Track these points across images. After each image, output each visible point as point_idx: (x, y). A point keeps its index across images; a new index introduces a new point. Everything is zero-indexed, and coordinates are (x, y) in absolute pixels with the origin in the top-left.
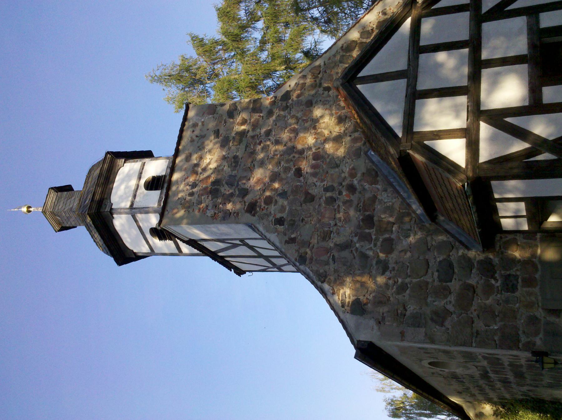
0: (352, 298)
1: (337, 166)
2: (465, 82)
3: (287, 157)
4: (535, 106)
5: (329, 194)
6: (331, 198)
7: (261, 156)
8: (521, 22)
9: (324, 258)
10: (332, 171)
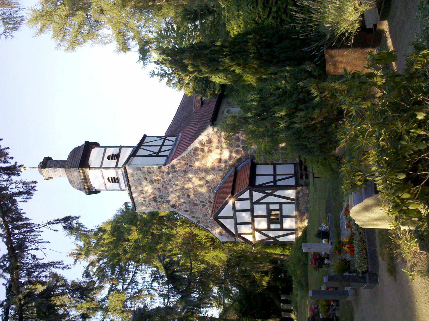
2: (250, 221)
4: (269, 229)
6: (204, 204)
7: (171, 190)
8: (264, 206)
9: (206, 221)
10: (202, 196)
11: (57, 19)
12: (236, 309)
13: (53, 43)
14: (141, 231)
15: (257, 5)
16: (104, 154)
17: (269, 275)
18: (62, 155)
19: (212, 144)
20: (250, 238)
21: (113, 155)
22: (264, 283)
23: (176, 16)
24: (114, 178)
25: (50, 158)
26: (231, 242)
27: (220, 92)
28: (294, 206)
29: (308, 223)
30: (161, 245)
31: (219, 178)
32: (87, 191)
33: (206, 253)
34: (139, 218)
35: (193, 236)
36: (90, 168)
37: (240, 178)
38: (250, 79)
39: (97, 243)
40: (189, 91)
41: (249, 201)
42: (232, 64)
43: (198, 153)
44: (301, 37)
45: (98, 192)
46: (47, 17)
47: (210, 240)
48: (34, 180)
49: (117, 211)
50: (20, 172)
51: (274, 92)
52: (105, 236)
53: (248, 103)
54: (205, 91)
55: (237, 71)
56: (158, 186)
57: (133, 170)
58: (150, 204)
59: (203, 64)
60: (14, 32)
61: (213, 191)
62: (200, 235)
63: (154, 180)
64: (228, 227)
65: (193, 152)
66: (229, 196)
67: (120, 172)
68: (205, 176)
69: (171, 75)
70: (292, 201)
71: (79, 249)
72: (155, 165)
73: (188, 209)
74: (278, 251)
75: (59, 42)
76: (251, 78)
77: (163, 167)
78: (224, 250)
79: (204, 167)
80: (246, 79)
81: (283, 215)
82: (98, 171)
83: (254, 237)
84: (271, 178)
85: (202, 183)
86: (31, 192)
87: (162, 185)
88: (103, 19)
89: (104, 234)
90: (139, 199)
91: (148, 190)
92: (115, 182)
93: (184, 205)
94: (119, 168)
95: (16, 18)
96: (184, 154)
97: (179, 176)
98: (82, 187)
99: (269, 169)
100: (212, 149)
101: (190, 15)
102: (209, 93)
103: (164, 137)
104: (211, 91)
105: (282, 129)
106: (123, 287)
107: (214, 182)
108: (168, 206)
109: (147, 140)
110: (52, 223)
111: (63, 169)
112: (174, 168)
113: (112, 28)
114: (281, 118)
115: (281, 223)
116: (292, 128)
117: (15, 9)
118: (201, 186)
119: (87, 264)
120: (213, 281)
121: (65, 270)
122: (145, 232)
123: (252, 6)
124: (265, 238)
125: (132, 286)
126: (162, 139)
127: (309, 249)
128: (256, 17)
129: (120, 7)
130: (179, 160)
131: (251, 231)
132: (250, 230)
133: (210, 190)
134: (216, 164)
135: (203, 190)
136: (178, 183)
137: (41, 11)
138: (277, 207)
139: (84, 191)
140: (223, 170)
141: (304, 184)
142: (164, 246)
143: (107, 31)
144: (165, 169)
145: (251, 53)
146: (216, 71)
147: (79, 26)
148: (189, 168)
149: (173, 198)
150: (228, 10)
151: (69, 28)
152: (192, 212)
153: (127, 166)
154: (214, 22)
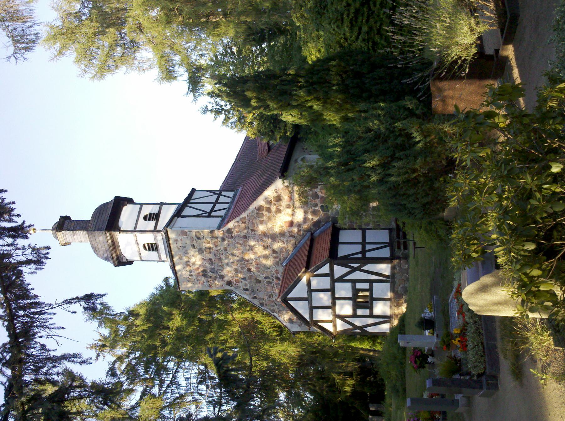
1: (269, 269)
4: (355, 316)
5: (267, 280)
7: (226, 261)
8: (349, 285)
9: (272, 304)
10: (267, 270)
13: (76, 69)
14: (185, 316)
16: (139, 214)
18: (85, 213)
19: (281, 202)
20: (329, 327)
21: (150, 214)
22: (347, 389)
24: (152, 244)
25: (68, 218)
27: (293, 135)
28: (388, 285)
29: (407, 308)
30: (212, 335)
31: (290, 247)
33: (270, 347)
34: (183, 298)
35: (254, 324)
36: (120, 231)
37: (317, 247)
38: (332, 118)
39: (127, 331)
40: (252, 133)
41: (328, 278)
42: (309, 98)
44: (399, 66)
45: (130, 263)
46: (69, 36)
47: (277, 329)
48: (46, 245)
50: (28, 235)
51: (364, 135)
52: (138, 322)
54: (273, 132)
55: (315, 107)
56: (209, 256)
57: (176, 235)
58: (198, 280)
59: (271, 98)
60: (27, 52)
61: (281, 264)
62: (264, 322)
63: (204, 248)
65: (256, 211)
66: (303, 270)
68: (272, 244)
69: (228, 111)
70: (386, 279)
71: (102, 339)
73: (248, 287)
74: (366, 345)
77: (216, 232)
79: (271, 232)
80: (328, 118)
81: (374, 296)
82: (130, 236)
83: (335, 326)
84: (359, 248)
85: (267, 252)
86: (43, 260)
90: (184, 272)
91: (195, 262)
92: (153, 250)
93: (244, 282)
94: (159, 231)
96: (244, 215)
97: (237, 243)
98: (110, 256)
99: (356, 236)
100: (281, 208)
101: (255, 35)
103: (218, 192)
104: (281, 132)
105: (373, 183)
106: (160, 390)
108: (222, 283)
109: (196, 195)
110: (69, 303)
112: (231, 233)
115: (371, 308)
116: (386, 182)
117: (29, 24)
118: (266, 257)
119: (113, 359)
121: (83, 365)
123: (336, 24)
124: (350, 327)
126: (216, 194)
130: (238, 222)
131: (330, 318)
132: (329, 316)
133: (278, 262)
134: (286, 228)
135: (269, 262)
136: (236, 252)
137: (61, 27)
138: (366, 286)
139: (112, 261)
140: (296, 236)
141: (401, 256)
142: (215, 336)
143: (146, 54)
144: (219, 233)
145: (334, 85)
146: (287, 106)
149: (228, 272)
150: (305, 29)
151: (96, 51)
152: (253, 291)
153: (169, 230)
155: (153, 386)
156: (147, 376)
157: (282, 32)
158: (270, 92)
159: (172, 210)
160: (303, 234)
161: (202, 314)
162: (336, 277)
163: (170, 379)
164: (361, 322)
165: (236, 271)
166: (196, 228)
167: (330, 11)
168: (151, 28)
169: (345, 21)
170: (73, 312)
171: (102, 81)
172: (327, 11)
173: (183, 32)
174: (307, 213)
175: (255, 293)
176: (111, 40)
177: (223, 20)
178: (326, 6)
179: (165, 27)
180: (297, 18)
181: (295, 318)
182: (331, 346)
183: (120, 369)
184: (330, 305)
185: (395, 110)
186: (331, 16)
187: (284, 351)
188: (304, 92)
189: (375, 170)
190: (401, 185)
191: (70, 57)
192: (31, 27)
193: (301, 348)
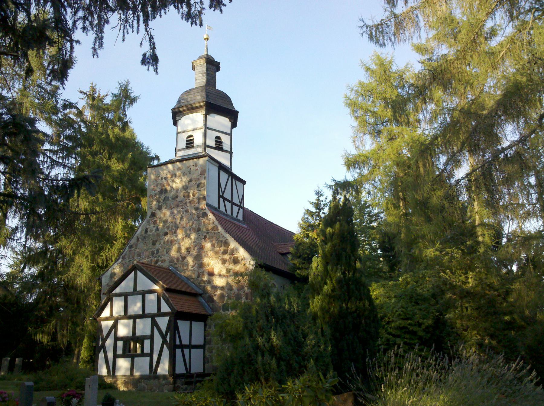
0: (116, 272)
1: (167, 253)
3: (174, 225)
4: (117, 339)
7: (176, 212)
8: (149, 333)
9: (131, 257)
10: (165, 251)
11: (381, 88)
12: (5, 297)
13: (354, 83)
14: (122, 173)
15: (403, 319)
17: (50, 343)
18: (222, 83)
19: (233, 264)
20: (106, 313)
21: (222, 142)
22: (39, 336)
23: (388, 224)
24: (193, 143)
25: (218, 69)
26: (100, 291)
27: (297, 276)
28: (147, 372)
29: (123, 391)
30: (101, 199)
31: (187, 274)
32: (176, 110)
33: (87, 257)
34: (140, 173)
35: (110, 240)
36: (206, 115)
37: (187, 299)
38: (316, 303)
39: (107, 120)
40: (299, 237)
41: (156, 311)
42: (334, 282)
43: (221, 246)
44: (367, 360)
45: (175, 123)
46: (383, 77)
47: (105, 263)
48: (204, 23)
49: (148, 147)
50: (213, 9)
51: (300, 331)
52: (116, 130)
53: (288, 299)
54: (299, 257)
55: (326, 287)
56: (181, 195)
57: (201, 165)
58: (157, 185)
59: (334, 246)
60: (368, 36)
61: (171, 265)
62: (113, 250)
63: (189, 191)
64: (123, 284)
65: (224, 240)
66: (165, 285)
67: (200, 150)
68: (191, 255)
69: (318, 215)
70: (153, 370)
71: (100, 98)
72: (208, 192)
73: (149, 233)
74: (84, 354)
75: (355, 89)
76: (316, 306)
77: (204, 202)
78: (90, 281)
79: (203, 254)
80: (315, 300)
81: (135, 358)
82: (201, 124)
83: (107, 319)
84: (185, 342)
85: (183, 250)
86: (190, 20)
87: (181, 201)
88: (383, 140)
89: (119, 129)
90: (165, 172)
91: (176, 183)
92: (187, 144)
93: (154, 229)
94: (205, 150)
95: (383, 39)
96: (220, 229)
97: (193, 223)
98: (182, 105)
99: (198, 339)
100: (227, 264)
101: (388, 243)
102: (296, 262)
103: (242, 205)
104: (300, 264)
105: (255, 340)
106: (46, 150)
107: (183, 266)
108: (154, 208)
109: (239, 183)
110: (150, 41)
111: (205, 84)
112: (203, 217)
113: (372, 150)
114: (269, 340)
115: (123, 356)
116: (256, 353)
117: (393, 38)
118: (179, 250)
119: (80, 107)
120: (46, 267)
121: (92, 50)
122: (121, 178)
123: (402, 313)
124: (105, 335)
125: (47, 162)
126: (241, 203)
127: (90, 386)
128: (389, 318)
129: (397, 160)
130: (214, 223)
131: (115, 314)
132: (117, 313)
133: (173, 261)
135: (173, 253)
136: (184, 221)
137: (391, 70)
138: (147, 350)
139: (177, 106)
140: (200, 279)
141: (176, 385)
142: (100, 203)
143: (369, 144)
144: (203, 205)
145: (347, 305)
146: (326, 261)
147: (374, 112)
148: (203, 234)
149: (165, 214)
150: (396, 285)
151: (371, 100)
152: (145, 238)
153: (207, 158)
154: (380, 273)
155: (52, 143)
156: (62, 138)
157: (392, 268)
158: (339, 246)
159: (225, 162)
160: (201, 286)
161: (123, 190)
162: (158, 319)
163: (57, 160)
164: (110, 345)
165: (165, 222)
166: (208, 184)
167: (414, 307)
168: (392, 148)
169: (406, 321)
170: (141, 44)
171: (344, 104)
172: (413, 306)
173: (389, 176)
174: (222, 290)
175: (143, 240)
176: (380, 113)
177: (401, 213)
178: (417, 304)
179: (394, 161)
180: (406, 278)
181: (116, 280)
182: (84, 318)
183: (70, 113)
184: (128, 314)
185: (324, 361)
186: (409, 309)
187: (82, 270)
188: (339, 276)
189: (268, 342)
190: (252, 367)
191: (364, 78)
192: (391, 40)
193: (84, 287)
